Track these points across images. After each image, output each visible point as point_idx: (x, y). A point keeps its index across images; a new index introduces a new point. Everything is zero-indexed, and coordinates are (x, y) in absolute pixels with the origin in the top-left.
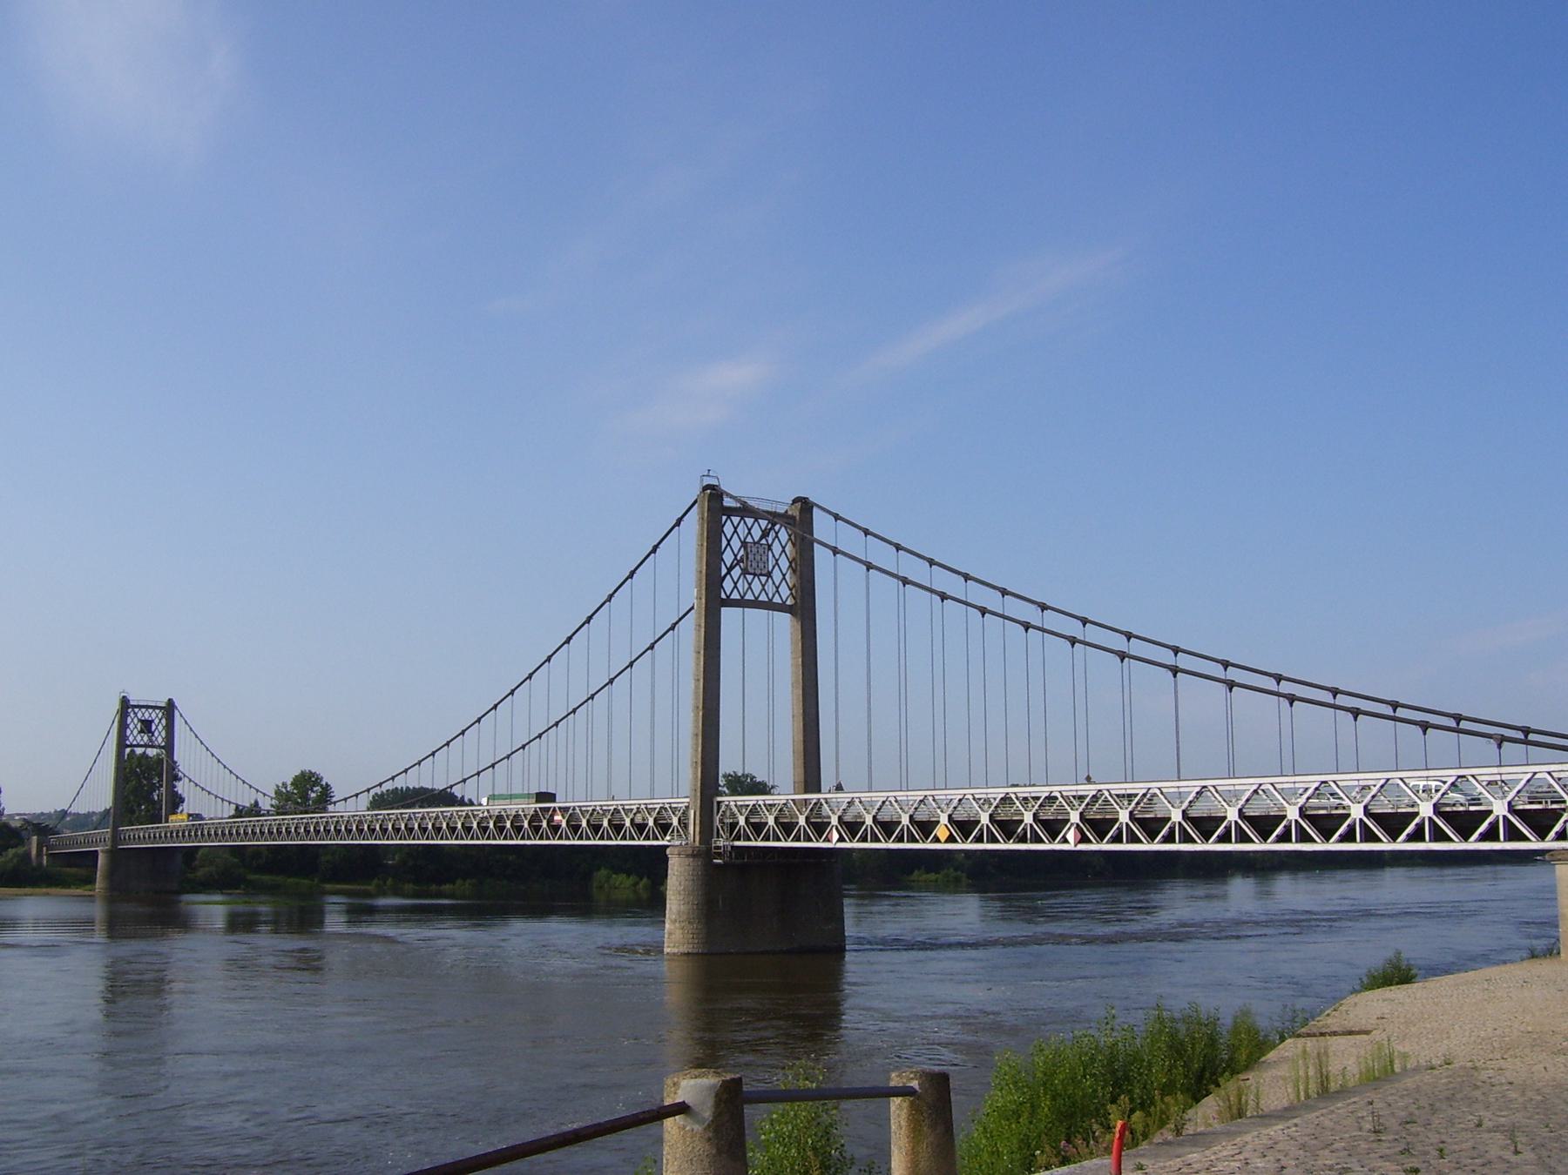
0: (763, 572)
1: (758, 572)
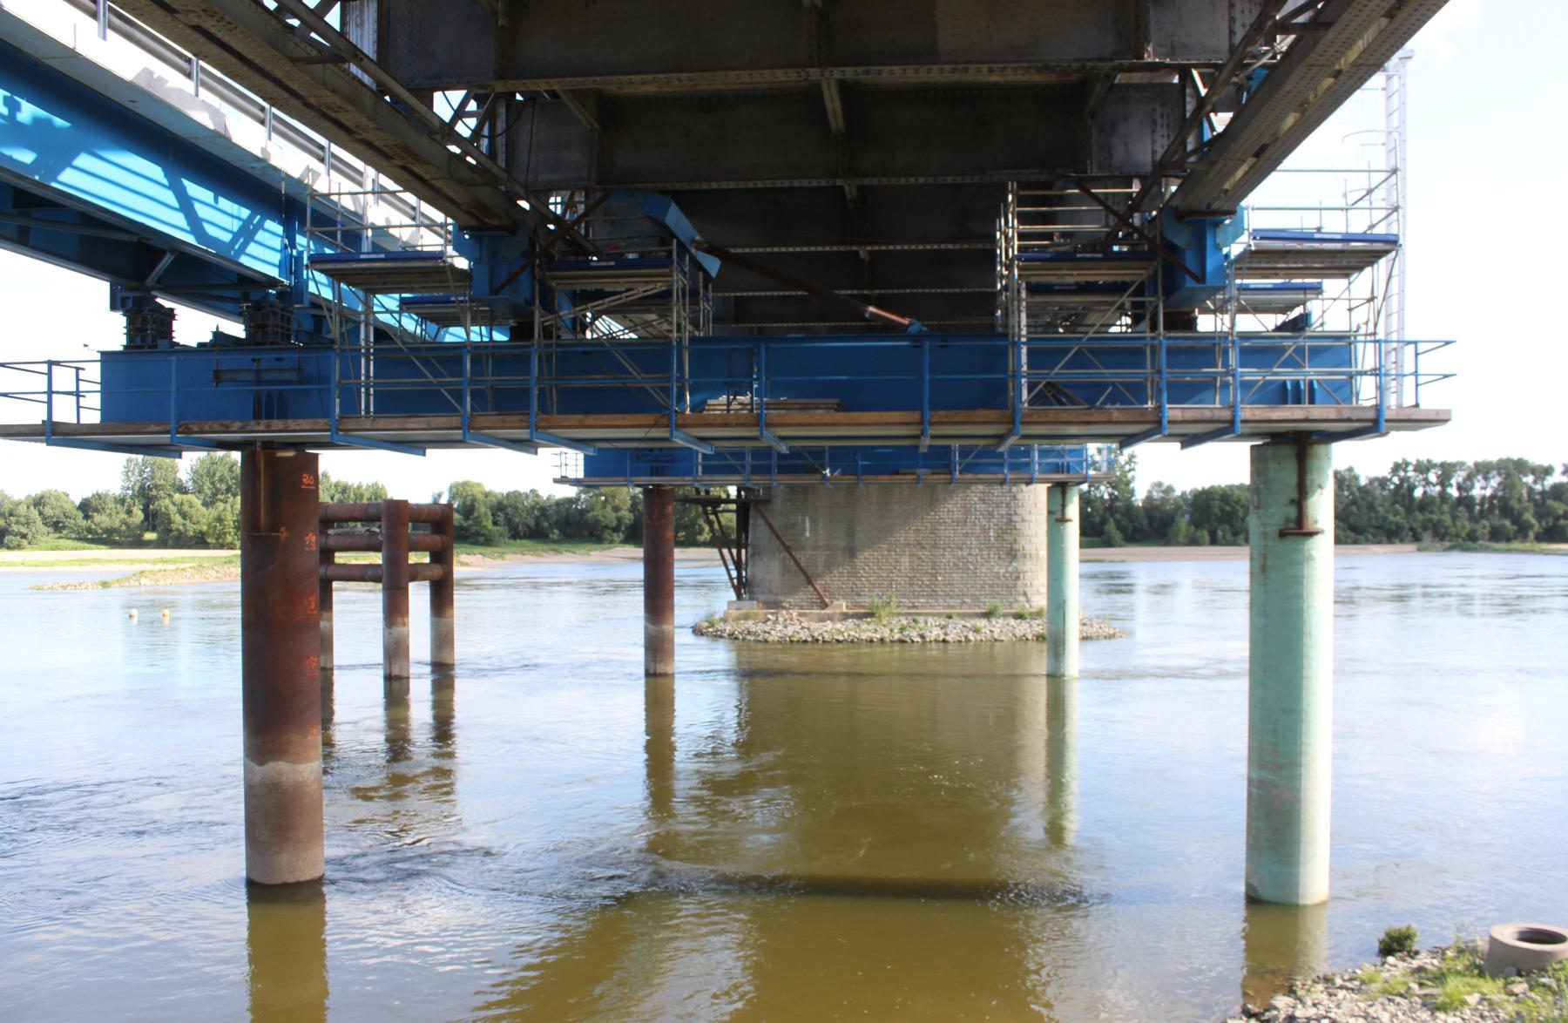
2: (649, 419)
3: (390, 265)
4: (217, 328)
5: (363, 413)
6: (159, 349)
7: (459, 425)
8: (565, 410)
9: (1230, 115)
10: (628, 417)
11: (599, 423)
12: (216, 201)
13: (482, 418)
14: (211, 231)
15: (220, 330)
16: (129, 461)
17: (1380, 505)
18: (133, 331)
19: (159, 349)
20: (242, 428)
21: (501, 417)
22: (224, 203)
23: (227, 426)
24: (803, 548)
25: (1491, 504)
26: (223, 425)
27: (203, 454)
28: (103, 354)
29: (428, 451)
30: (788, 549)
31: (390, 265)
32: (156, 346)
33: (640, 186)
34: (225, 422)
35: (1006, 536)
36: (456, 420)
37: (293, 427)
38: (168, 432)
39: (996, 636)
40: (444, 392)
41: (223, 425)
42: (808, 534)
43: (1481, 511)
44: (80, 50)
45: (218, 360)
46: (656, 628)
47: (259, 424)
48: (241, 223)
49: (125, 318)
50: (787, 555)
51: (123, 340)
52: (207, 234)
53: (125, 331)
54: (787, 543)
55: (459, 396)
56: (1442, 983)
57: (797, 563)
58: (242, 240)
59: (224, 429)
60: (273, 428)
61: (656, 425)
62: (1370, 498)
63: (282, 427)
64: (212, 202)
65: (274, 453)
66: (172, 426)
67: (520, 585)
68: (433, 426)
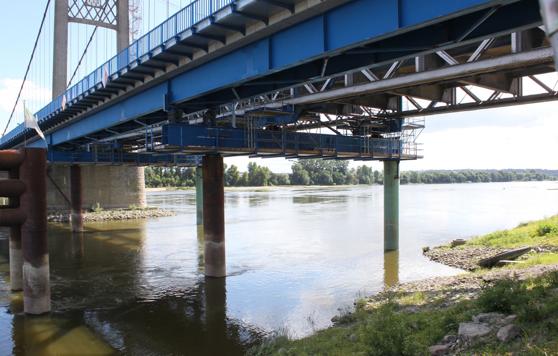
0: (97, 6)
1: (94, 5)
9: (431, 101)
17: (152, 175)
23: (231, 149)
24: (63, 188)
25: (186, 174)
30: (58, 188)
35: (133, 183)
37: (247, 150)
39: (129, 217)
42: (65, 183)
43: (183, 177)
44: (111, 29)
46: (78, 215)
47: (238, 149)
50: (58, 190)
54: (58, 186)
55: (281, 144)
56: (400, 298)
57: (61, 192)
62: (149, 172)
63: (244, 150)
67: (286, 198)
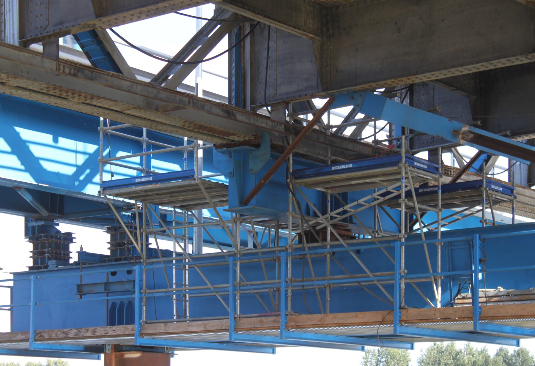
2: (377, 316)
3: (158, 186)
4: (81, 248)
5: (175, 318)
6: (49, 269)
7: (470, 316)
8: (337, 309)
10: (360, 314)
11: (336, 321)
12: (56, 140)
13: (246, 320)
14: (48, 166)
15: (84, 250)
16: (48, 361)
18: (37, 254)
19: (49, 269)
20: (76, 335)
21: (259, 319)
22: (63, 142)
23: (67, 334)
26: (64, 333)
27: (430, 344)
28: (15, 274)
29: (277, 349)
31: (158, 186)
32: (47, 267)
33: (358, 88)
34: (65, 330)
36: (225, 323)
38: (278, 328)
40: (219, 297)
41: (64, 333)
45: (81, 276)
48: (87, 157)
49: (30, 246)
51: (30, 263)
52: (45, 171)
53: (31, 254)
58: (88, 171)
59: (65, 336)
60: (97, 334)
61: (382, 322)
64: (52, 143)
65: (123, 355)
66: (31, 335)
68: (208, 328)
